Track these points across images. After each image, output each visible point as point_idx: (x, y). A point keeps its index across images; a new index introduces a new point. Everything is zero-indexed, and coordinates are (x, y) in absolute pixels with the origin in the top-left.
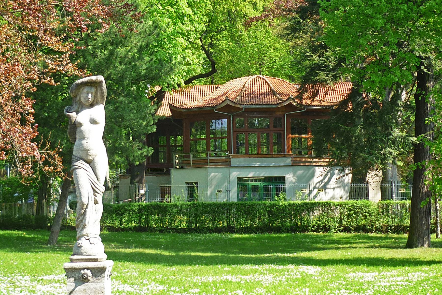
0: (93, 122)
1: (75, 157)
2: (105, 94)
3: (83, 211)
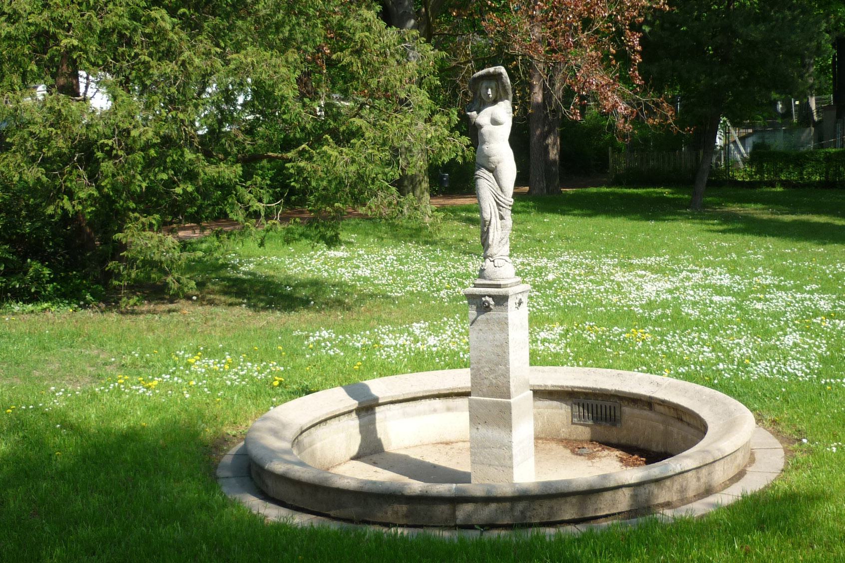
0: (495, 122)
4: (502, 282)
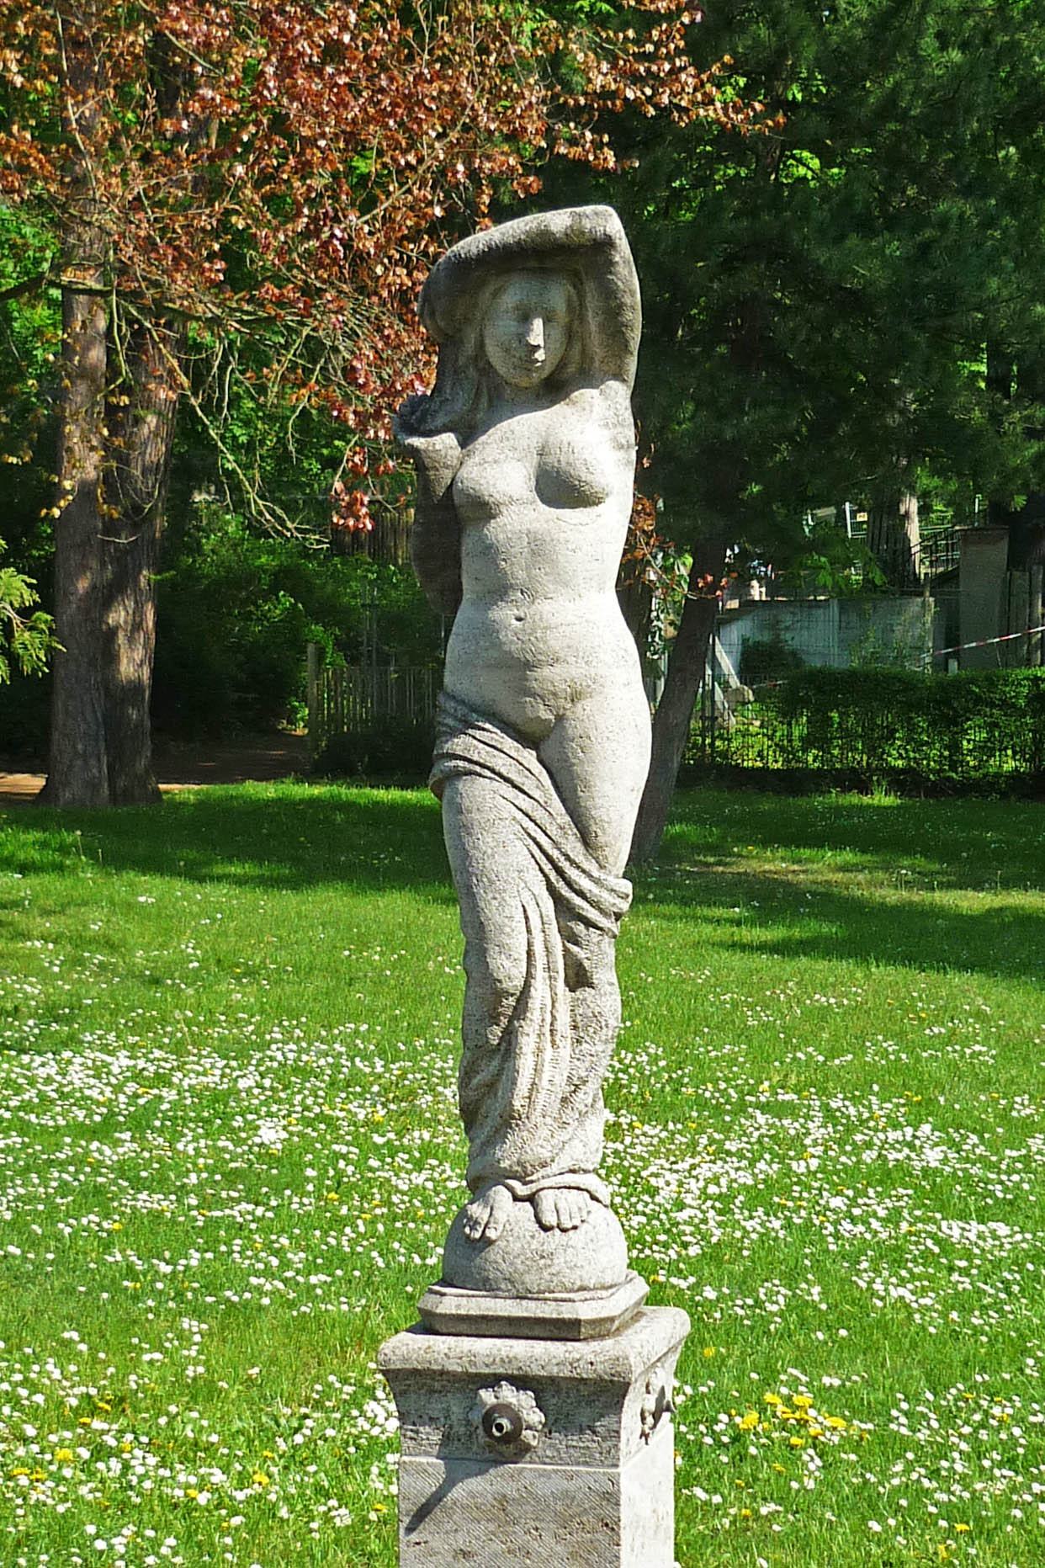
1: (450, 705)
2: (634, 318)
3: (498, 1031)
4: (585, 1311)
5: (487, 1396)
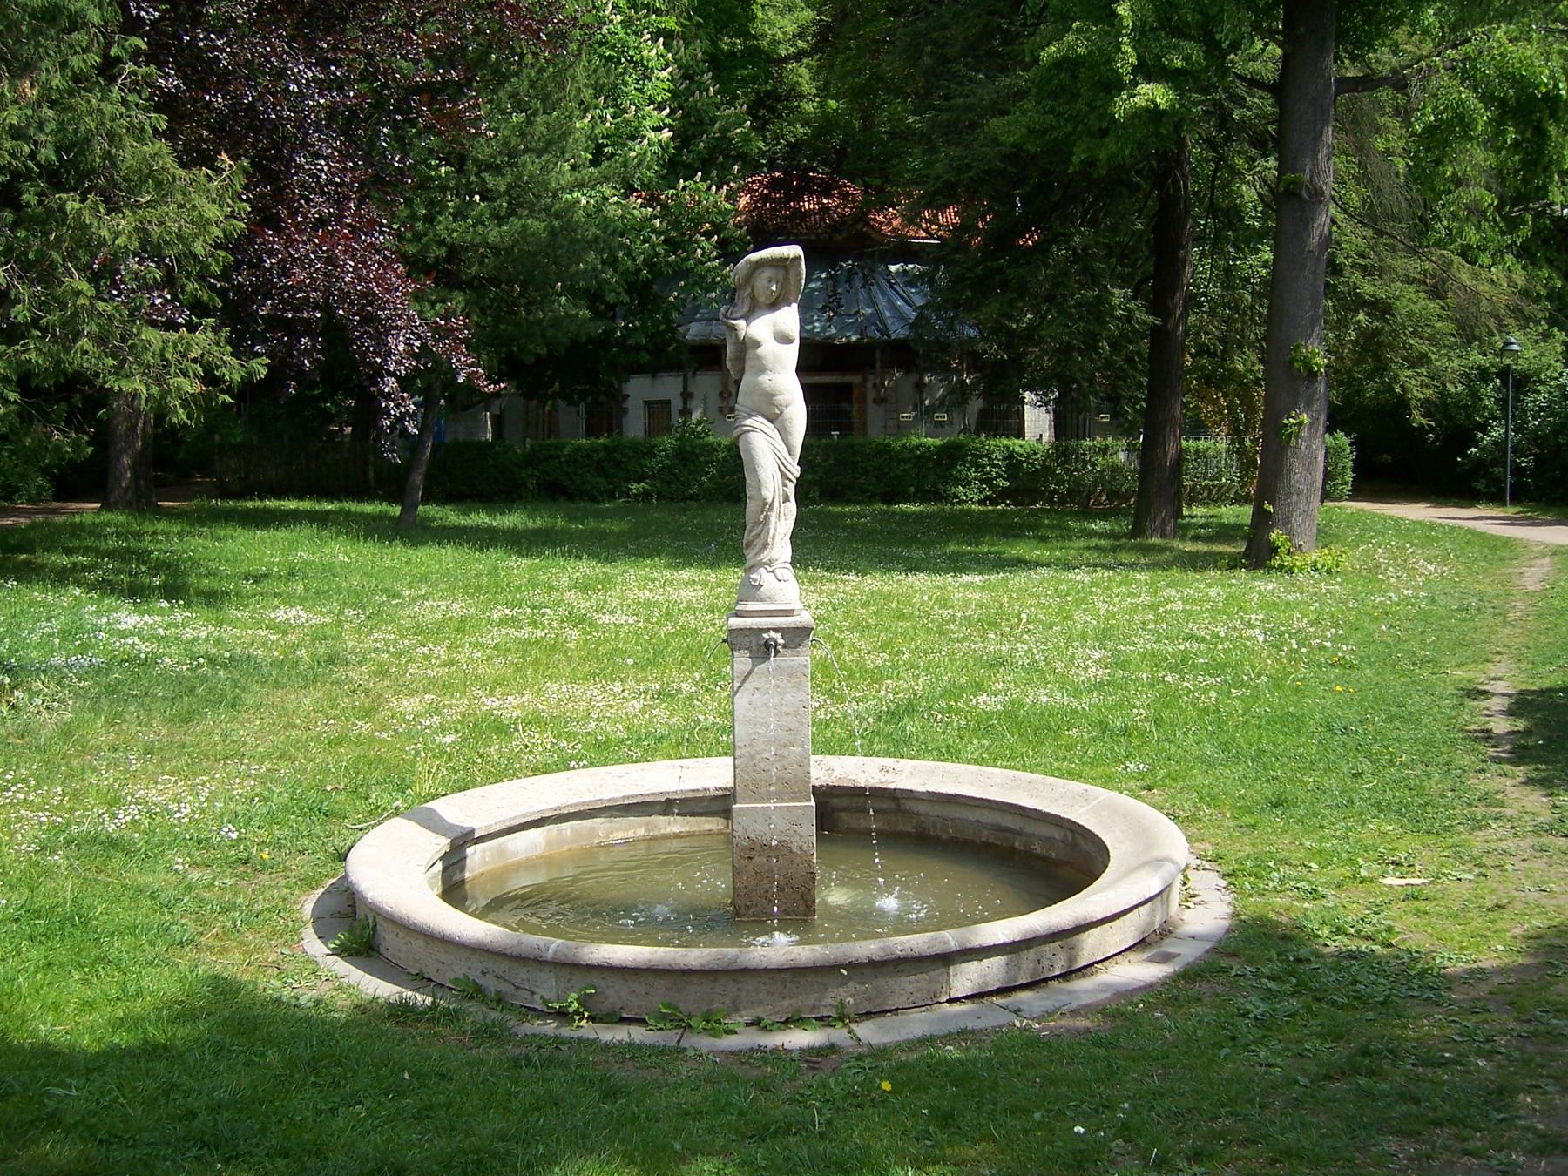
0: (784, 339)
5: (766, 636)
